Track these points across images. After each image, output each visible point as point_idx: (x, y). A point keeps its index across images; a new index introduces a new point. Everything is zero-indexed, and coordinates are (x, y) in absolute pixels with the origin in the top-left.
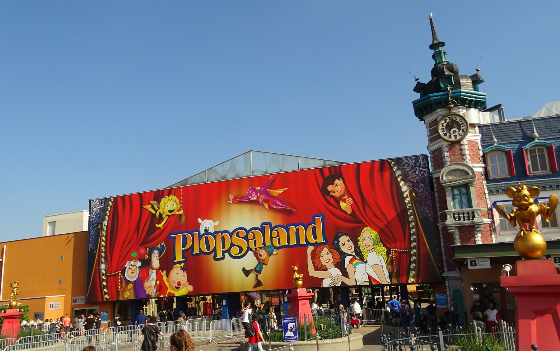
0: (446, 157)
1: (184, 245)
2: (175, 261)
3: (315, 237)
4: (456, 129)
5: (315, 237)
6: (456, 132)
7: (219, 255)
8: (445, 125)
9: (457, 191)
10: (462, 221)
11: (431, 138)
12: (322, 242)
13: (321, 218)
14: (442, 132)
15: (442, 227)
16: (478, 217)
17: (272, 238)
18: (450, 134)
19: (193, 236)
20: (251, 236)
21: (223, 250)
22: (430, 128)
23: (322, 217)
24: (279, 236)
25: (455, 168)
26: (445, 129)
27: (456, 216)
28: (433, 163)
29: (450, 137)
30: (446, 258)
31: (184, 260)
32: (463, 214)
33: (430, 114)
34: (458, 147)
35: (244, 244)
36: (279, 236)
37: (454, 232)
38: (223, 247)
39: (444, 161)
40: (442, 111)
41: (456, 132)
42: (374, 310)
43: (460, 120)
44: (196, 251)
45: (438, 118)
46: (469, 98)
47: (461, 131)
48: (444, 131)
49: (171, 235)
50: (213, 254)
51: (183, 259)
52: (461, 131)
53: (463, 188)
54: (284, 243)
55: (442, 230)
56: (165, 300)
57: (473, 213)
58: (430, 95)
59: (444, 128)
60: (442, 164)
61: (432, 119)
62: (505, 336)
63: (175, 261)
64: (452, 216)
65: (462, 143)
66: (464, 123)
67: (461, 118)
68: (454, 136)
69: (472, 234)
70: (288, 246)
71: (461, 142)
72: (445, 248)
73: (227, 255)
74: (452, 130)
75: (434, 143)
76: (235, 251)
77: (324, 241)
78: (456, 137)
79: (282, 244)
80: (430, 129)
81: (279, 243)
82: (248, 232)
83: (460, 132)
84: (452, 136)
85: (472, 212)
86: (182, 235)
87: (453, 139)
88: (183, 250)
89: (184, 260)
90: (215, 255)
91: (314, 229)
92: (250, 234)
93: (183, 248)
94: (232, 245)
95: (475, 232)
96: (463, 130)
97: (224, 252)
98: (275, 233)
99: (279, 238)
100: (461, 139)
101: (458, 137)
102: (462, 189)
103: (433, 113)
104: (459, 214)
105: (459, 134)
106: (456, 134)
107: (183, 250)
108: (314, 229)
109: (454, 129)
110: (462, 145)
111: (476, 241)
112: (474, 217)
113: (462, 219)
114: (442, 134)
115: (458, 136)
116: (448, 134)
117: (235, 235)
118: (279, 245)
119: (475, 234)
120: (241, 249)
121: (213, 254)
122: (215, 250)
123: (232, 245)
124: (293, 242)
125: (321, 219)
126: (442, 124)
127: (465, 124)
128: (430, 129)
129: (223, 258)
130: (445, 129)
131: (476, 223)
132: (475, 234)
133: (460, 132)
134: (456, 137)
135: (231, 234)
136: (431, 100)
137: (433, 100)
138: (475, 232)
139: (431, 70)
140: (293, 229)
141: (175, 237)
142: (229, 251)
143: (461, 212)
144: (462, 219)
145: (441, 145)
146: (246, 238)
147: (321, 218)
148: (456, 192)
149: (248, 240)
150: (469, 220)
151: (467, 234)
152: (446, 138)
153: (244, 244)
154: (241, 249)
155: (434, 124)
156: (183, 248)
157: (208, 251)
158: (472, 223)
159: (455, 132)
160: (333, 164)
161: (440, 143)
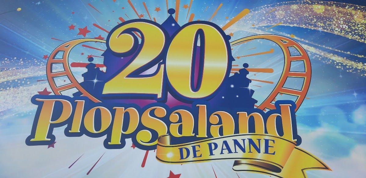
2: (32, 140)
7: (116, 139)
13: (290, 106)
17: (209, 125)
24: (181, 122)
31: (50, 140)
36: (181, 122)
38: (125, 128)
50: (105, 137)
51: (47, 138)
63: (32, 140)
73: (129, 141)
76: (144, 137)
86: (56, 102)
89: (50, 140)
93: (51, 121)
94: (141, 127)
97: (124, 137)
121: (105, 137)
122: (109, 132)
123: (141, 127)
142: (133, 136)
146: (166, 120)
147: (290, 106)
149: (168, 123)
156: (51, 121)
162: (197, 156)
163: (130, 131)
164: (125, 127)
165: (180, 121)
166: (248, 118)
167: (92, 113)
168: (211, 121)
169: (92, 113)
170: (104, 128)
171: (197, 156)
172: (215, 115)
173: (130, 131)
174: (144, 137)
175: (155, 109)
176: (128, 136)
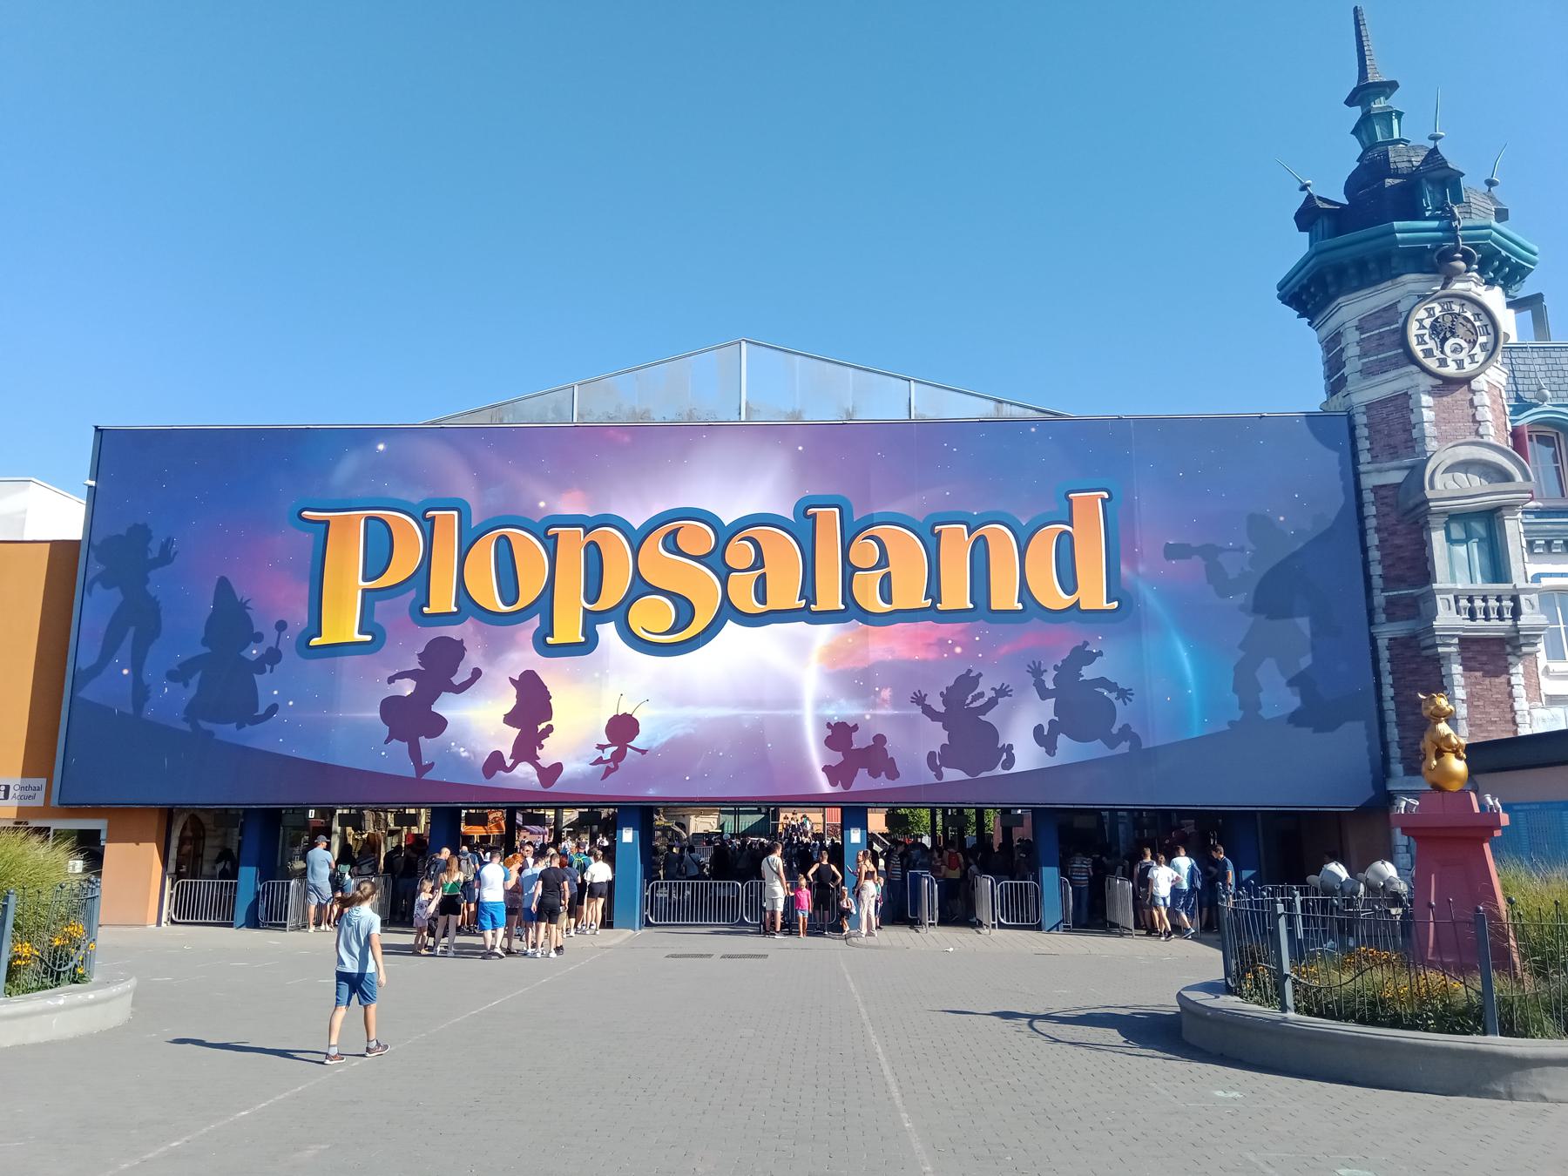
0: (1425, 424)
1: (377, 562)
2: (315, 642)
3: (1069, 584)
4: (1462, 341)
5: (1069, 584)
6: (1462, 349)
7: (568, 629)
8: (1427, 323)
9: (1459, 528)
10: (1480, 623)
11: (1363, 364)
12: (1105, 606)
13: (1103, 500)
14: (1419, 344)
15: (1390, 639)
16: (1532, 614)
17: (849, 570)
18: (1442, 352)
19: (427, 525)
20: (739, 553)
21: (588, 606)
22: (1362, 334)
23: (1106, 496)
24: (887, 565)
25: (1469, 457)
26: (1426, 338)
27: (1464, 603)
28: (1368, 442)
29: (1443, 363)
30: (1399, 734)
31: (369, 638)
32: (1499, 599)
33: (1372, 289)
34: (1461, 394)
35: (705, 591)
36: (887, 565)
37: (1449, 654)
38: (593, 592)
39: (1414, 436)
40: (1418, 281)
41: (1462, 349)
42: (1006, 884)
43: (1474, 315)
44: (443, 599)
45: (1399, 301)
46: (1504, 253)
47: (1477, 349)
48: (1426, 343)
49: (306, 513)
50: (535, 622)
51: (361, 632)
52: (1477, 349)
53: (1477, 521)
54: (911, 594)
55: (1388, 648)
56: (307, 833)
57: (1515, 599)
58: (1397, 225)
59: (1424, 335)
60: (1410, 444)
61: (1375, 304)
62: (280, 847)
63: (315, 642)
64: (1453, 603)
65: (1474, 385)
66: (1486, 326)
67: (1478, 310)
68: (1455, 361)
69: (1501, 663)
70: (933, 613)
71: (1472, 382)
72: (1398, 705)
74: (1451, 341)
75: (1376, 380)
76: (652, 616)
77: (1116, 604)
78: (1460, 364)
79: (899, 603)
80: (1363, 336)
81: (887, 599)
82: (726, 534)
83: (1472, 352)
84: (1449, 361)
85: (1510, 597)
86: (368, 518)
87: (1451, 370)
88: (365, 591)
89: (369, 638)
90: (548, 628)
91: (1065, 547)
92: (735, 542)
93: (365, 579)
94: (641, 587)
95: (1511, 659)
96: (1483, 346)
97: (592, 620)
98: (864, 553)
99: (888, 575)
100: (1473, 373)
101: (1469, 367)
102: (1473, 524)
103: (1382, 286)
104: (1470, 600)
105: (1472, 357)
106: (1463, 355)
107: (365, 591)
108: (1065, 547)
109: (1458, 340)
110: (1474, 392)
111: (1512, 687)
112: (1516, 612)
113: (1480, 615)
114: (1418, 350)
115: (1467, 361)
116: (1437, 353)
117: (655, 545)
118: (886, 608)
119: (1511, 664)
120: (685, 610)
121: (535, 622)
122: (545, 604)
123: (641, 587)
124: (957, 595)
125: (1099, 501)
126: (1420, 321)
127: (1490, 329)
128: (1363, 336)
129: (589, 643)
130: (1426, 338)
131: (1527, 629)
132: (1511, 664)
133: (1472, 352)
134: (1460, 364)
135: (637, 540)
136: (1396, 242)
137: (1404, 241)
138: (1511, 659)
139: (1343, 190)
140: (956, 543)
141: (327, 523)
142: (619, 615)
143: (1464, 593)
144: (1480, 615)
145: (1412, 384)
147: (1103, 500)
148: (1457, 531)
149: (724, 573)
150: (1501, 618)
151: (1486, 664)
152: (1432, 364)
153: (705, 591)
154: (685, 610)
155: (1379, 322)
156: (365, 579)
157: (506, 604)
158: (1513, 629)
159: (1457, 349)
160: (1013, 413)
161: (1407, 378)
162: (49, 544)
163: (612, 595)
164: (593, 589)
165: (759, 562)
166: (968, 541)
167: (485, 553)
168: (854, 559)
169: (485, 553)
170: (527, 595)
171: (49, 544)
172: (741, 540)
173: (612, 595)
174: (652, 616)
175: (678, 529)
176: (603, 617)
